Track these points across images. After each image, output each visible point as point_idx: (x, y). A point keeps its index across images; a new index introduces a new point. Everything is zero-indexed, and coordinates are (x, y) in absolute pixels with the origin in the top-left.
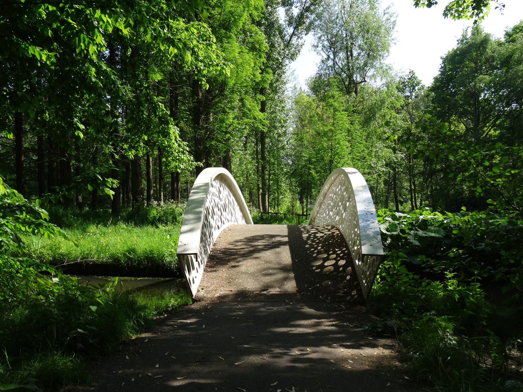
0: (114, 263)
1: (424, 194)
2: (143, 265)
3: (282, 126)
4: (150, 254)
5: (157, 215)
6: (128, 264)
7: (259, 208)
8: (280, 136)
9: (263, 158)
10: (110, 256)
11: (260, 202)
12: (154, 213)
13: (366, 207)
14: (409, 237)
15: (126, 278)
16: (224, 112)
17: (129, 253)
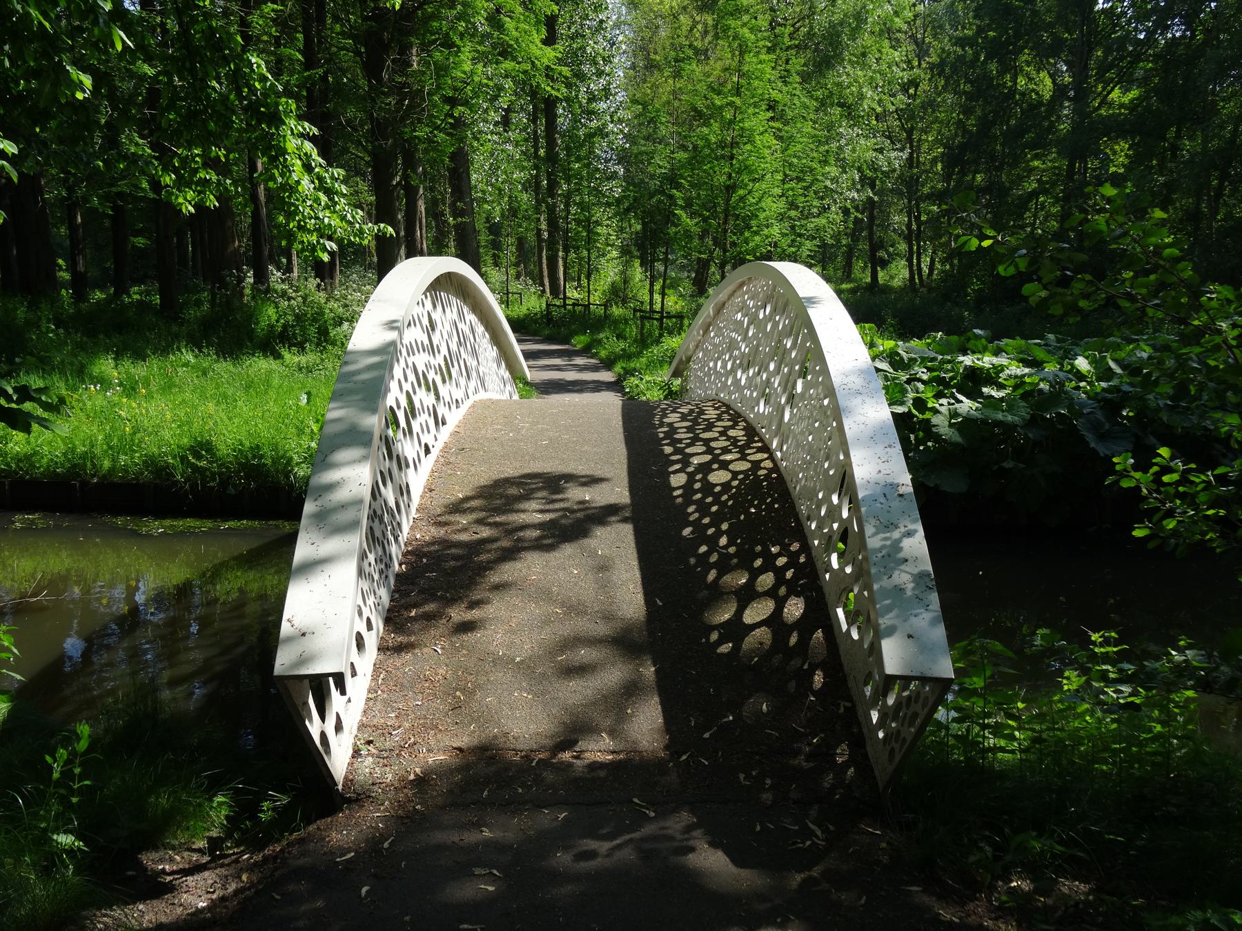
0: (158, 481)
1: (942, 245)
2: (235, 486)
3: (600, 74)
4: (254, 457)
5: (277, 321)
6: (194, 486)
7: (542, 284)
8: (592, 99)
9: (552, 158)
10: (145, 462)
11: (545, 266)
12: (270, 314)
13: (883, 467)
14: (936, 420)
15: (190, 522)
16: (448, 44)
17: (198, 457)
